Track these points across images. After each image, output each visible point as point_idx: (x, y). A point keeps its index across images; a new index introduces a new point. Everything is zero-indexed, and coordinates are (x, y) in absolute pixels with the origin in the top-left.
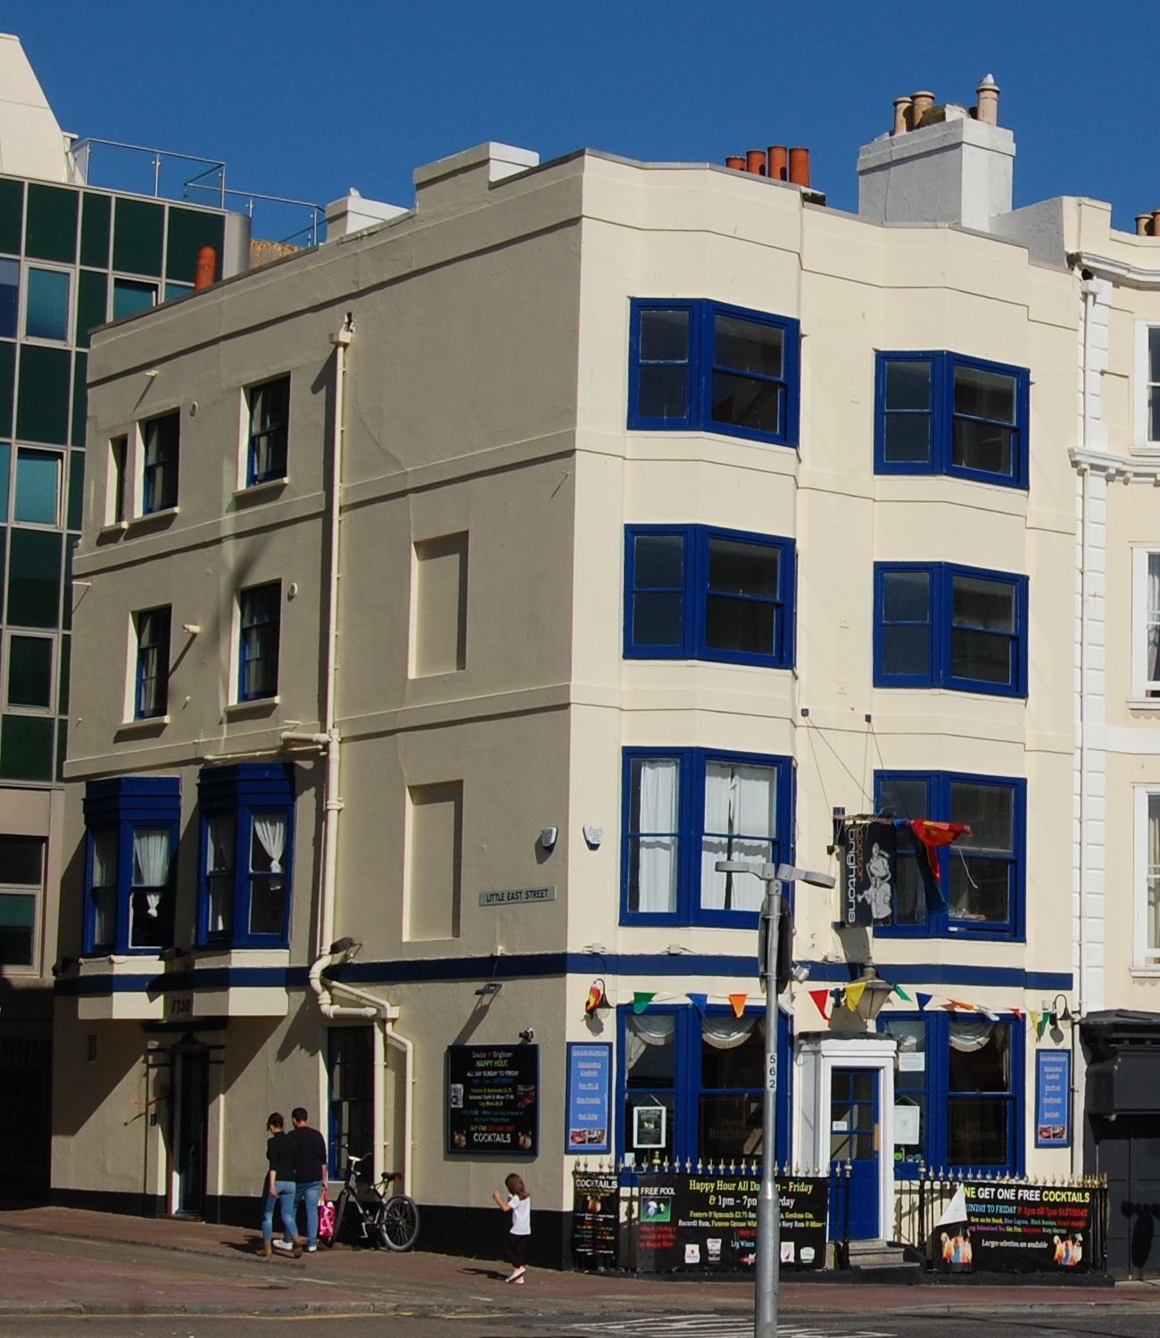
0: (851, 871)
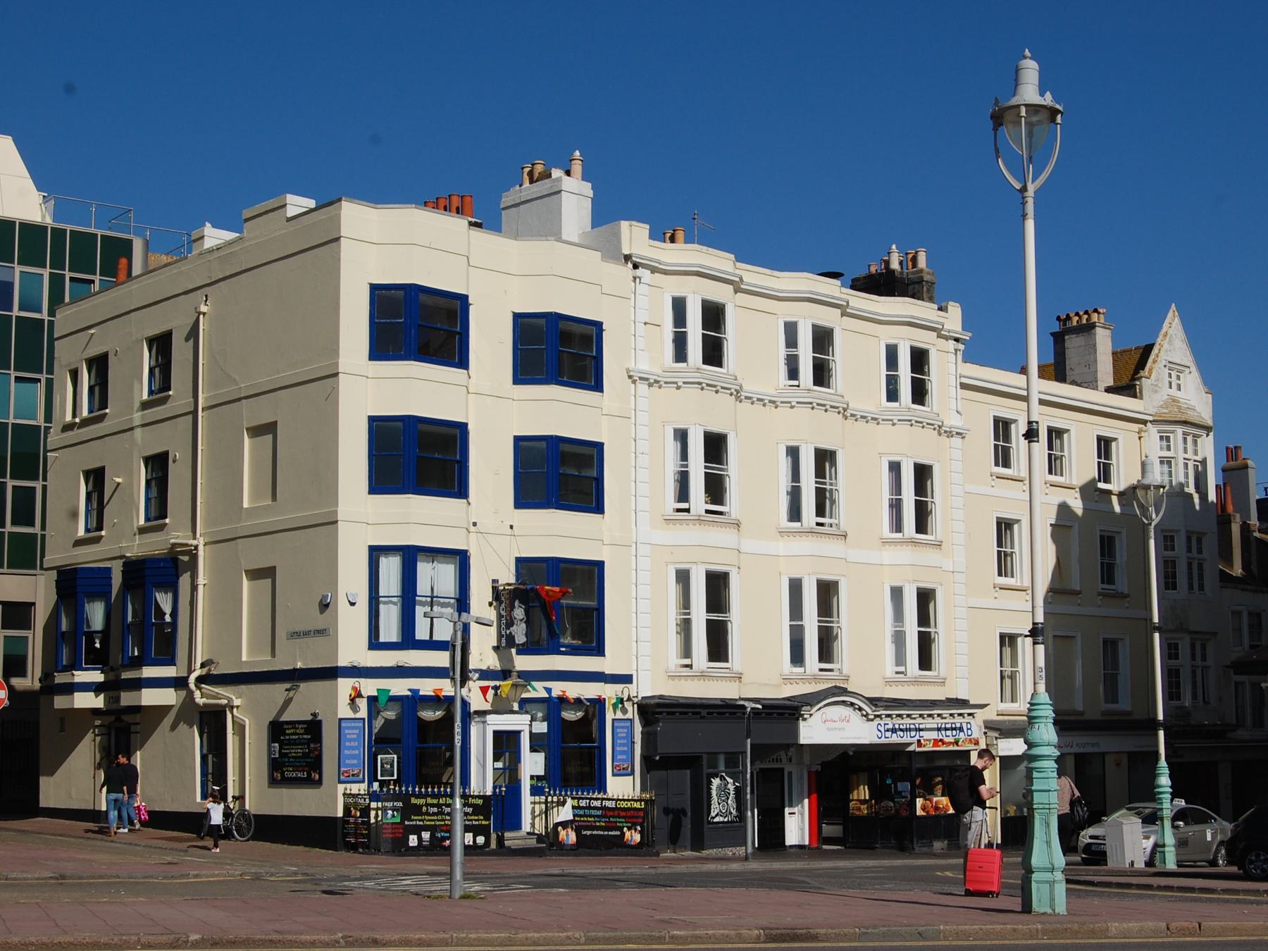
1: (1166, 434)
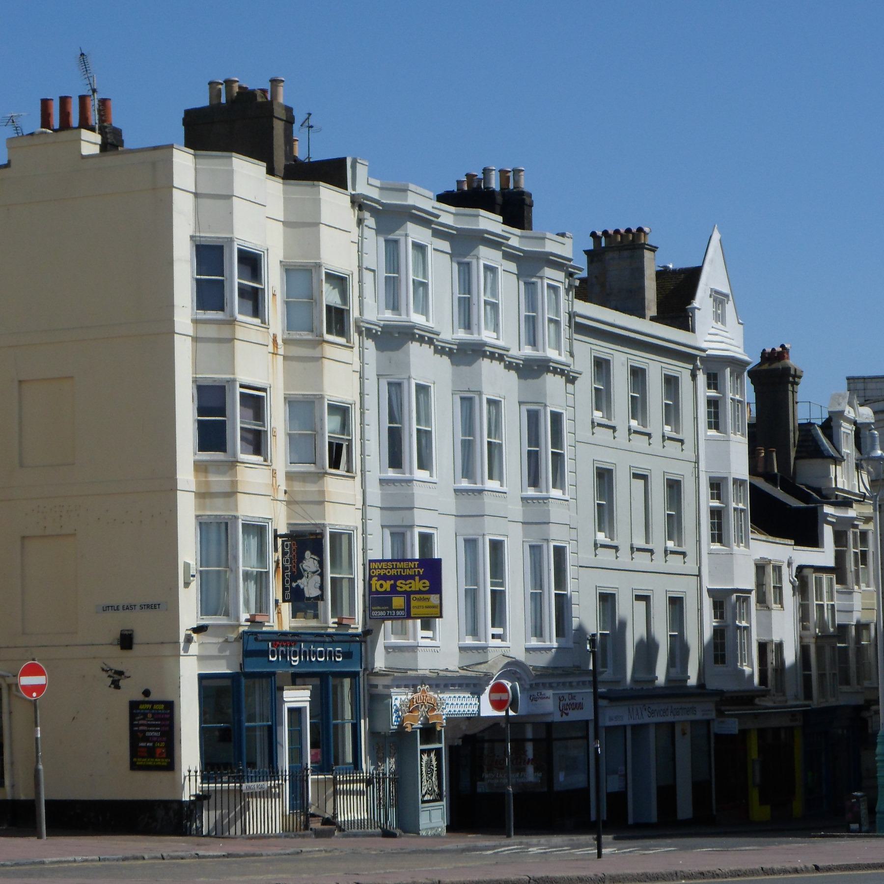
1: (449, 346)
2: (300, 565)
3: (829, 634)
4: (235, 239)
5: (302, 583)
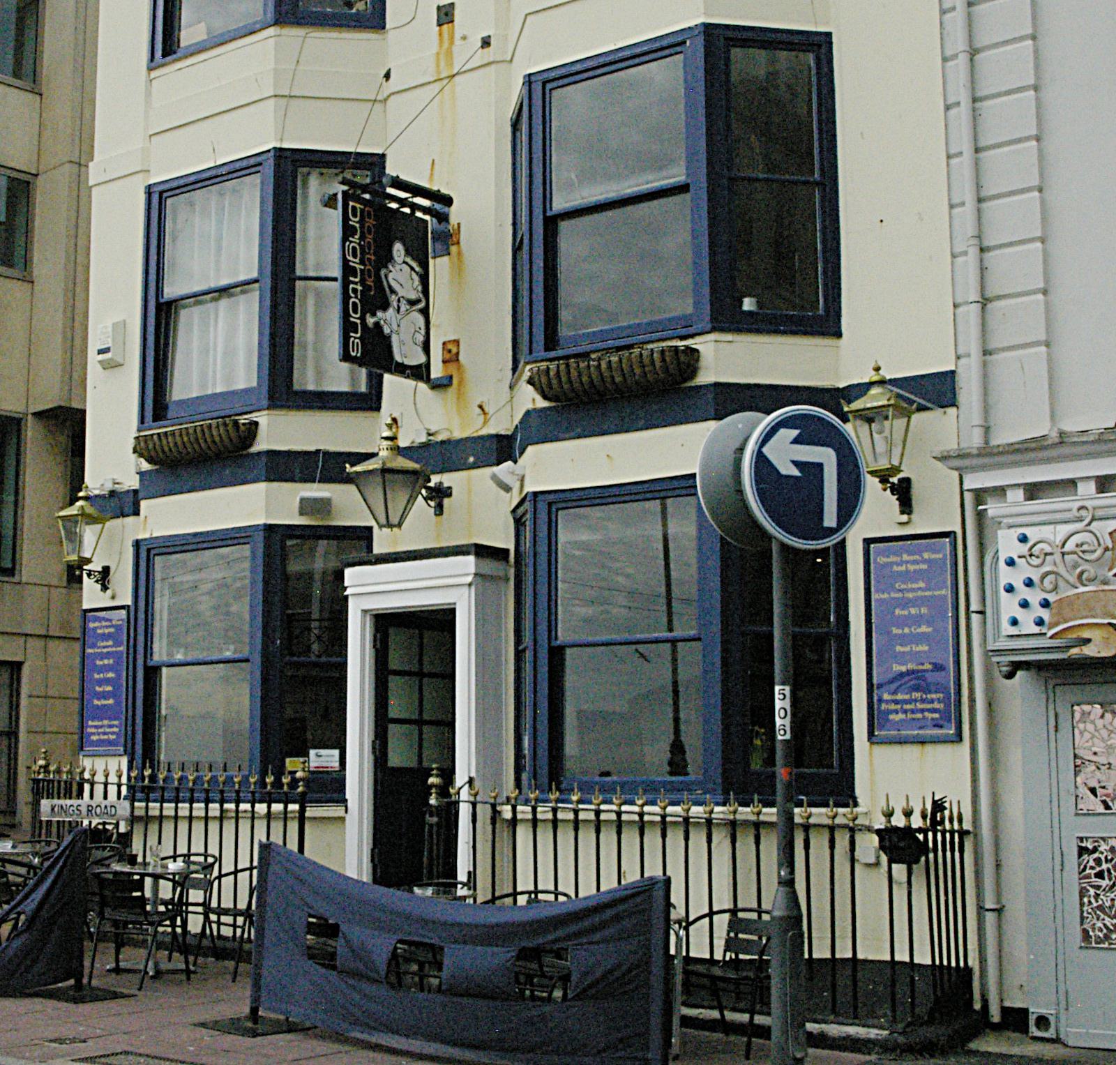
0: (353, 272)
2: (383, 272)
3: (265, 388)
4: (340, 935)
5: (388, 318)
